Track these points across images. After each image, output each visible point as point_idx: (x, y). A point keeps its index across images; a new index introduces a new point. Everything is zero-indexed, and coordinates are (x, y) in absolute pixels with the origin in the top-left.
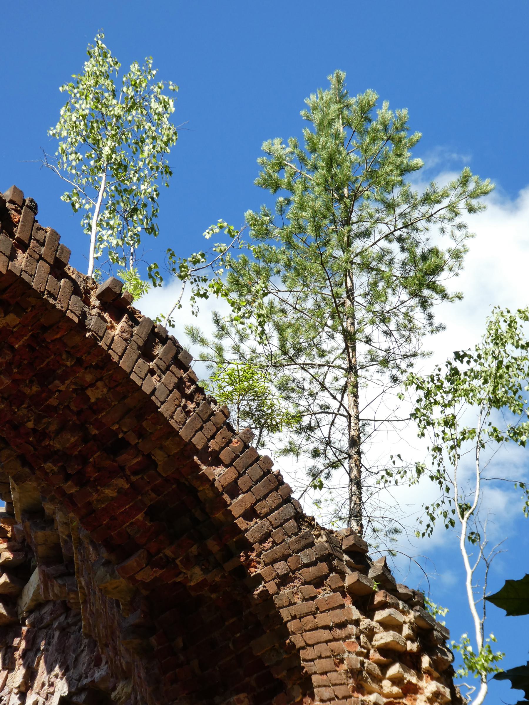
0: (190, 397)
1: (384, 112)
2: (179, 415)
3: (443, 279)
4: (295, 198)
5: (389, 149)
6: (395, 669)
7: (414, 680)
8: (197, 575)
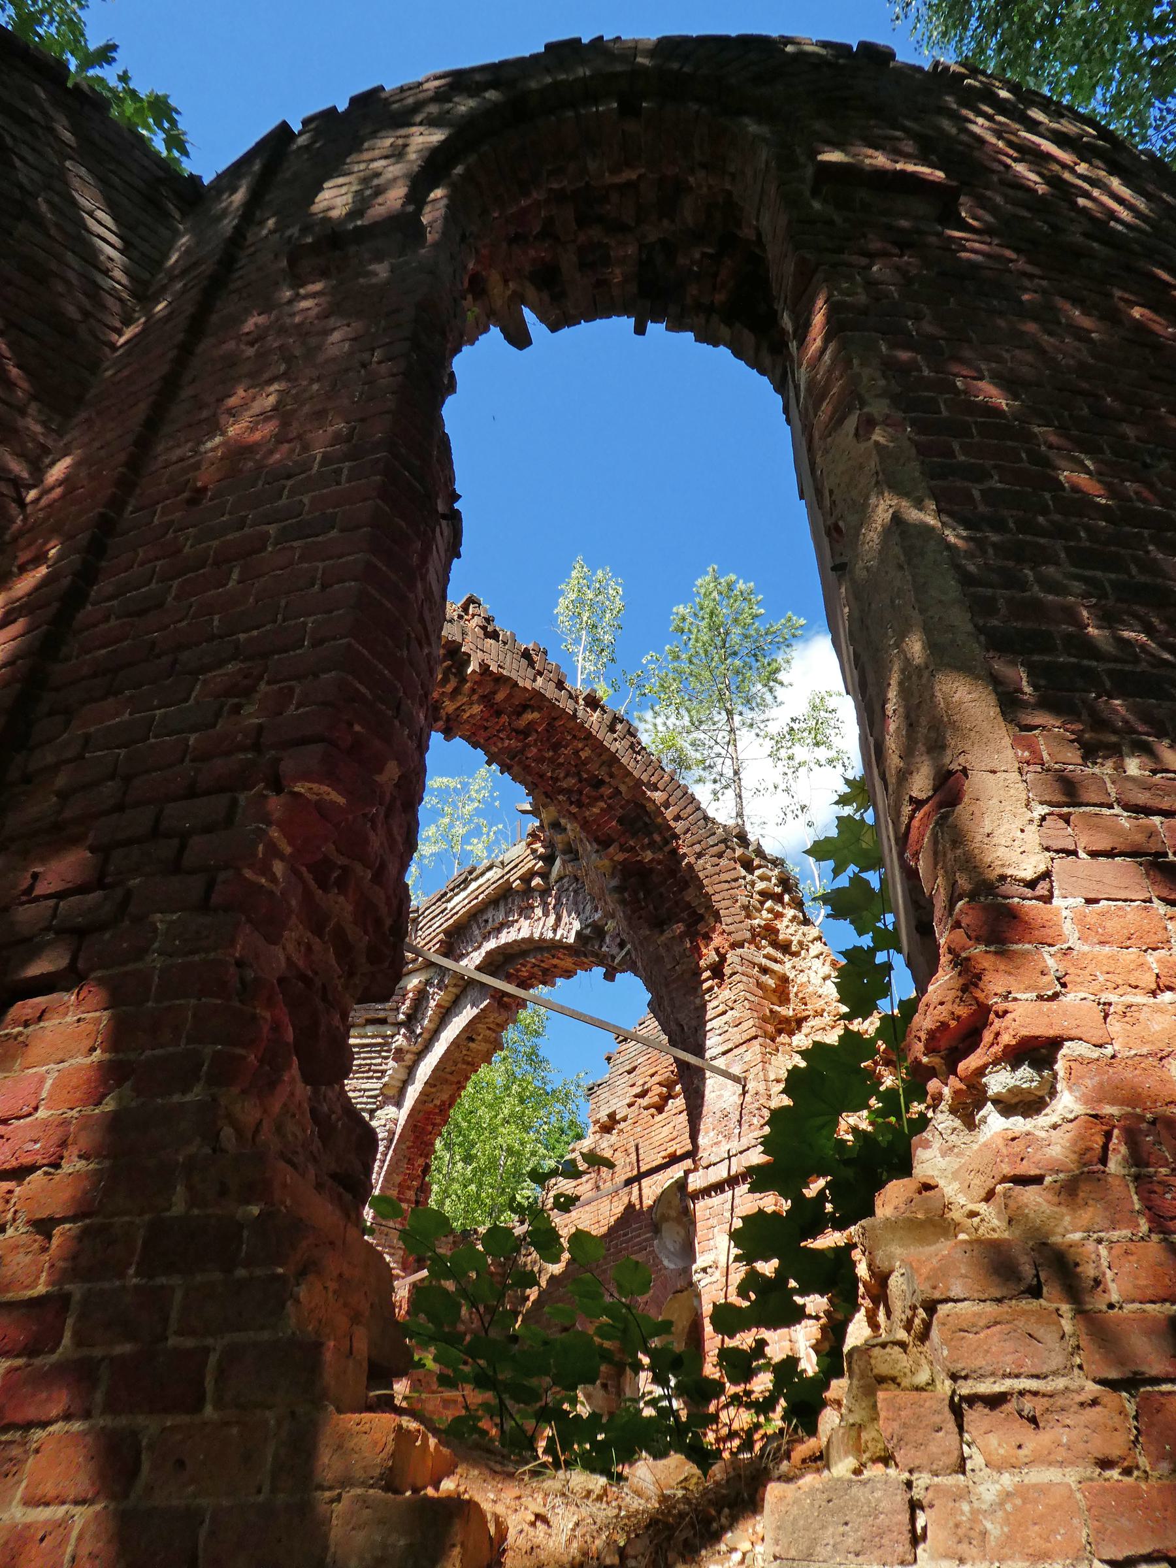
0: (638, 753)
1: (741, 585)
2: (632, 763)
3: (781, 676)
4: (693, 637)
5: (745, 605)
6: (769, 904)
7: (780, 909)
8: (648, 855)
